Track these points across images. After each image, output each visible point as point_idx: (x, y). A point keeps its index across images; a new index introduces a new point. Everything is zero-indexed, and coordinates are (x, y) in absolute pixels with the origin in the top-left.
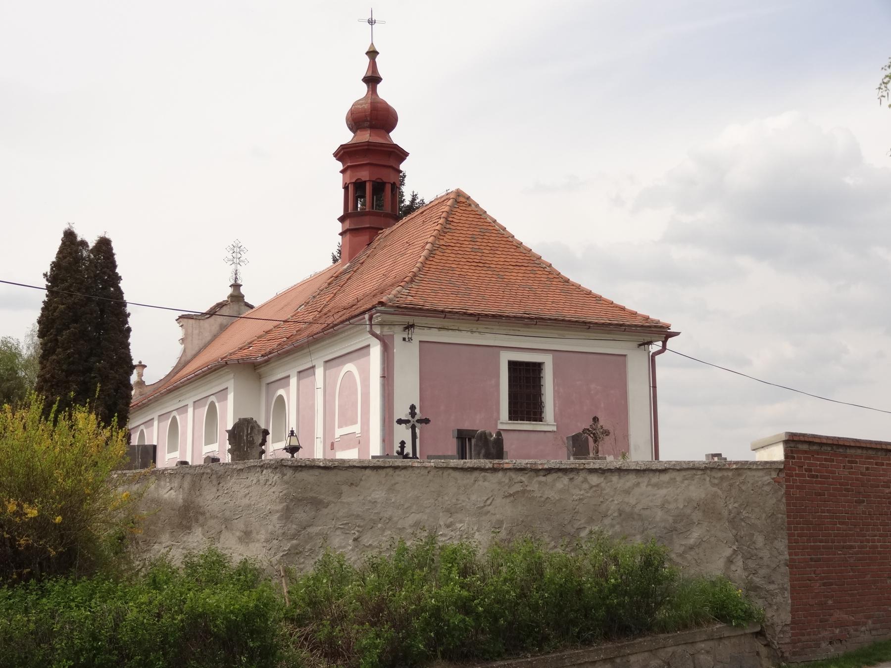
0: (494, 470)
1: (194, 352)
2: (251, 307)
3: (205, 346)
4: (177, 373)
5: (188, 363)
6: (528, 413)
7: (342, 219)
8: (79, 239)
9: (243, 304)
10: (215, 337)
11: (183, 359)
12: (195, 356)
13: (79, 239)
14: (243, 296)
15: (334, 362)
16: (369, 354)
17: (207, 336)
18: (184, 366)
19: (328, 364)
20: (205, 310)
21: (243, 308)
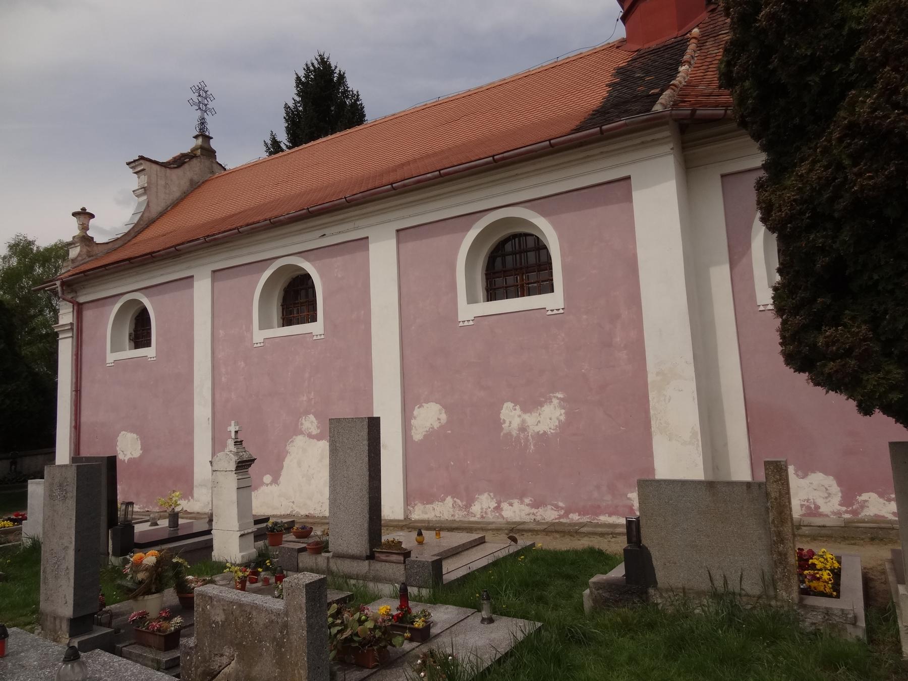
0: (697, 96)
1: (160, 209)
2: (225, 169)
3: (175, 204)
4: (140, 232)
5: (152, 222)
7: (342, 77)
8: (776, 235)
10: (185, 196)
11: (146, 215)
12: (162, 214)
13: (776, 235)
16: (192, 286)
17: (176, 193)
20: (161, 161)
21: (215, 165)
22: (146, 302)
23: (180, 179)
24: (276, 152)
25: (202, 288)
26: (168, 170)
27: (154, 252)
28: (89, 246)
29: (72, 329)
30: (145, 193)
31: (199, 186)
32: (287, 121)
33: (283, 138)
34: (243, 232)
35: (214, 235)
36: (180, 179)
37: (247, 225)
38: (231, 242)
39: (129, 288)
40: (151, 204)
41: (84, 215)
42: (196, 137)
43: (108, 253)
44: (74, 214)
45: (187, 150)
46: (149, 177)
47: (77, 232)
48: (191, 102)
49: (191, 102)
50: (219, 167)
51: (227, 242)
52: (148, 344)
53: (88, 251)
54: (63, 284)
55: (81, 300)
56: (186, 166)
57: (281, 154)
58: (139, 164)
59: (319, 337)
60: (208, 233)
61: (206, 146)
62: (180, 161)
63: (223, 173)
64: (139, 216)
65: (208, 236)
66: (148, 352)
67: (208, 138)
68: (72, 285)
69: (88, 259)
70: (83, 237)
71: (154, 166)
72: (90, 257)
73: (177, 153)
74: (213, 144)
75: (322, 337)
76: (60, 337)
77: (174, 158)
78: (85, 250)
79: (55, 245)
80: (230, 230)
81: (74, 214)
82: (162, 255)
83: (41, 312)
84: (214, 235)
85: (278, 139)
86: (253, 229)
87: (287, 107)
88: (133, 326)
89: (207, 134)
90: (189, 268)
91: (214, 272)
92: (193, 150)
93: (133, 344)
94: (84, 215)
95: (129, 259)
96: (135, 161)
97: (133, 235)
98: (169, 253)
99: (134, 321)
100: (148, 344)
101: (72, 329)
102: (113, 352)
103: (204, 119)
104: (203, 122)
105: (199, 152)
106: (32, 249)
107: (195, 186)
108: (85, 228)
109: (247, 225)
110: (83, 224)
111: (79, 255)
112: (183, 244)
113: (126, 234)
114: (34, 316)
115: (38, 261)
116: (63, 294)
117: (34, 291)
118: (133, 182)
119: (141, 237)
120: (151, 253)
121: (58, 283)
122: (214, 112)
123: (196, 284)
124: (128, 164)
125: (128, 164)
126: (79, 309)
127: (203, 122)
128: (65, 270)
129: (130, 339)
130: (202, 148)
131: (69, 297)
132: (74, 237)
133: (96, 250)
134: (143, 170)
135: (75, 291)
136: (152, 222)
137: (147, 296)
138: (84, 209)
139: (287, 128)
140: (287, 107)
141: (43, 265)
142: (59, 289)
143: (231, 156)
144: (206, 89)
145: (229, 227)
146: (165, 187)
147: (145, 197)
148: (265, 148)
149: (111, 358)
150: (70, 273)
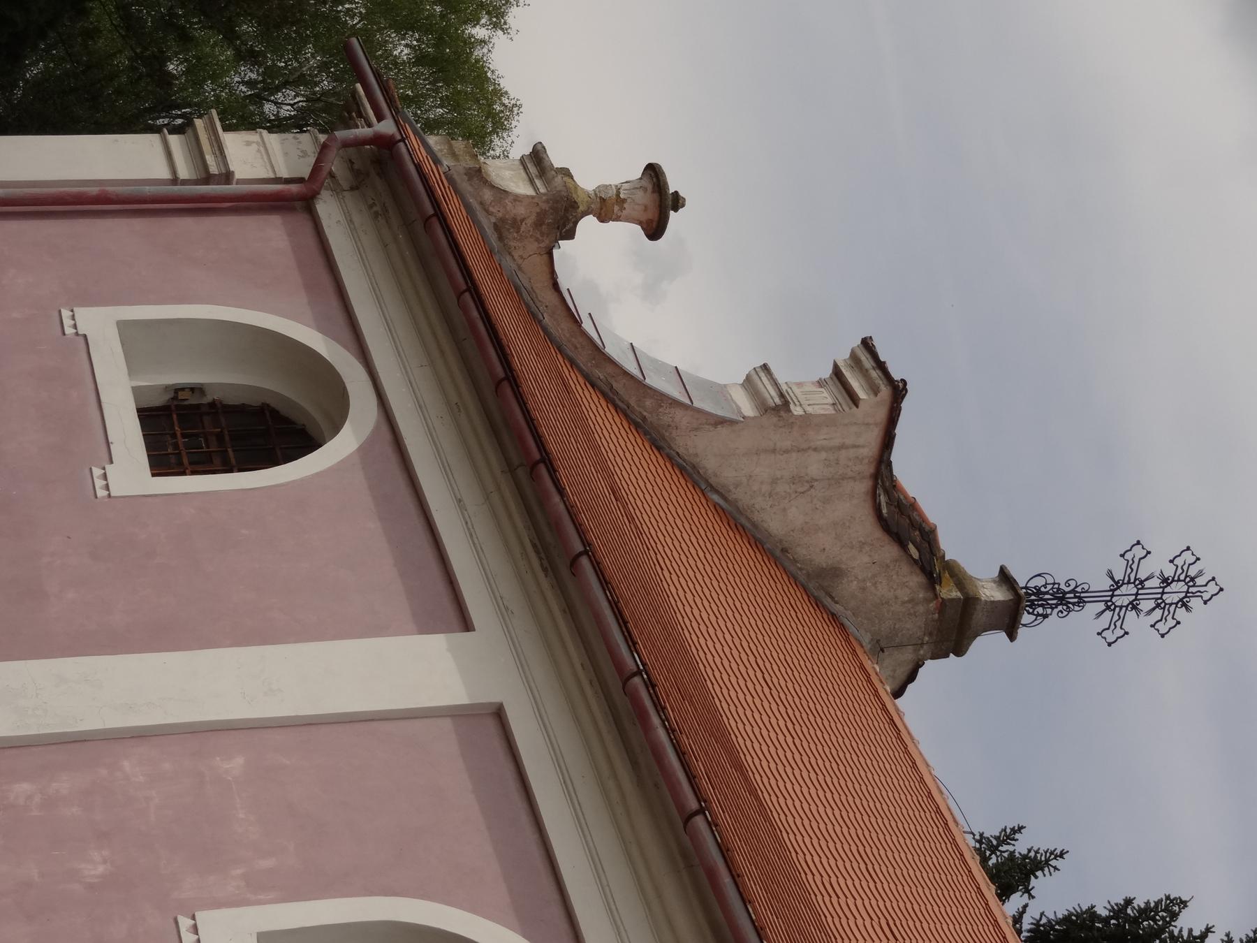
1: (710, 464)
2: (898, 693)
3: (736, 521)
4: (610, 397)
5: (657, 441)
6: (217, 461)
9: (547, 242)
10: (772, 553)
12: (690, 473)
14: (570, 235)
15: (319, 260)
16: (426, 625)
17: (778, 521)
18: (638, 425)
19: (491, 725)
20: (896, 457)
21: (908, 655)
22: (341, 447)
23: (835, 529)
24: (995, 875)
25: (422, 671)
26: (863, 486)
27: (552, 471)
28: (538, 224)
29: (207, 179)
30: (765, 408)
31: (818, 604)
32: (1119, 911)
33: (1051, 898)
34: (694, 837)
35: (660, 708)
36: (835, 529)
37: (724, 850)
38: (640, 782)
39: (391, 375)
40: (723, 431)
41: (655, 204)
42: (1005, 578)
43: (517, 292)
44: (653, 172)
45: (951, 546)
46: (827, 421)
47: (588, 180)
48: (1135, 552)
49: (1135, 552)
50: (902, 673)
51: (634, 764)
52: (162, 464)
53: (516, 223)
54: (385, 144)
55: (328, 209)
56: (890, 551)
57: (990, 891)
58: (875, 387)
59: (99, 483)
60: (660, 679)
61: (979, 616)
62: (903, 525)
63: (885, 690)
64: (674, 391)
65: (651, 685)
66: (128, 468)
67: (1008, 620)
68: (381, 173)
69: (487, 223)
70: (573, 205)
71: (872, 439)
72: (496, 227)
73: (933, 510)
74: (989, 644)
75: (101, 493)
76: (174, 140)
77: (913, 505)
78: (521, 211)
79: (499, 93)
80: (691, 778)
81: (653, 172)
82: (543, 501)
83: (252, 57)
84: (660, 708)
85: (1039, 883)
86: (712, 875)
87: (1173, 907)
88: (232, 399)
89: (1026, 618)
90: (503, 611)
91: (499, 714)
92: (953, 570)
93: (159, 400)
94: (655, 204)
95: (511, 378)
96: (881, 366)
97: (598, 373)
98: (557, 527)
99: (255, 401)
100: (162, 464)
101: (207, 179)
102: (117, 338)
103: (1081, 602)
104: (1065, 599)
105: (949, 592)
106: (476, 21)
107: (815, 588)
108: (607, 207)
109: (724, 850)
110: (621, 202)
111: (502, 193)
112: (605, 583)
113: (598, 352)
114: (231, 37)
115: (439, 43)
116: (346, 144)
117: (348, 49)
118: (803, 374)
119: (591, 402)
120: (547, 459)
121: (387, 127)
122: (1113, 636)
123: (437, 644)
124: (867, 344)
125: (867, 344)
126: (291, 201)
127: (1065, 599)
128: (438, 151)
129: (178, 390)
130: (969, 602)
131: (336, 165)
132: (566, 172)
133: (525, 251)
134: (854, 399)
135: (359, 182)
136: (657, 441)
137: (365, 450)
138: (677, 202)
139: (1091, 913)
140: (1173, 907)
141: (420, 59)
142: (362, 131)
143: (943, 705)
144: (1195, 603)
145: (700, 768)
146: (794, 480)
147: (748, 408)
148: (992, 831)
149: (99, 324)
150: (428, 166)
